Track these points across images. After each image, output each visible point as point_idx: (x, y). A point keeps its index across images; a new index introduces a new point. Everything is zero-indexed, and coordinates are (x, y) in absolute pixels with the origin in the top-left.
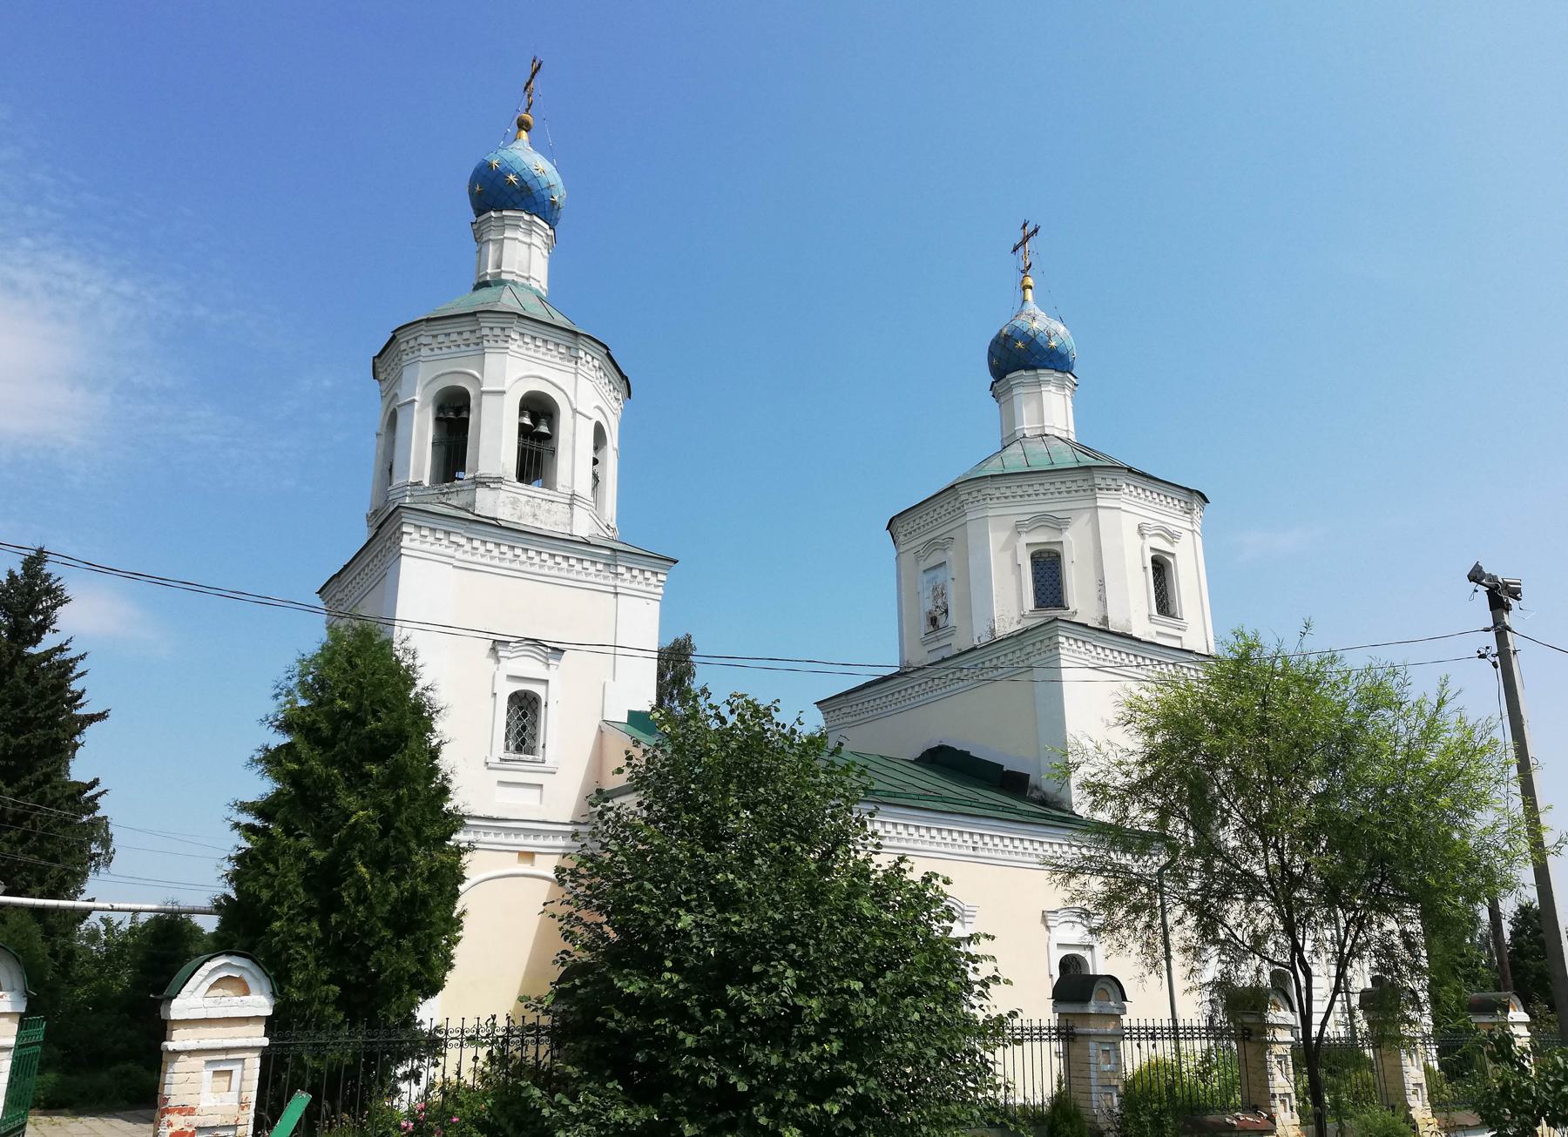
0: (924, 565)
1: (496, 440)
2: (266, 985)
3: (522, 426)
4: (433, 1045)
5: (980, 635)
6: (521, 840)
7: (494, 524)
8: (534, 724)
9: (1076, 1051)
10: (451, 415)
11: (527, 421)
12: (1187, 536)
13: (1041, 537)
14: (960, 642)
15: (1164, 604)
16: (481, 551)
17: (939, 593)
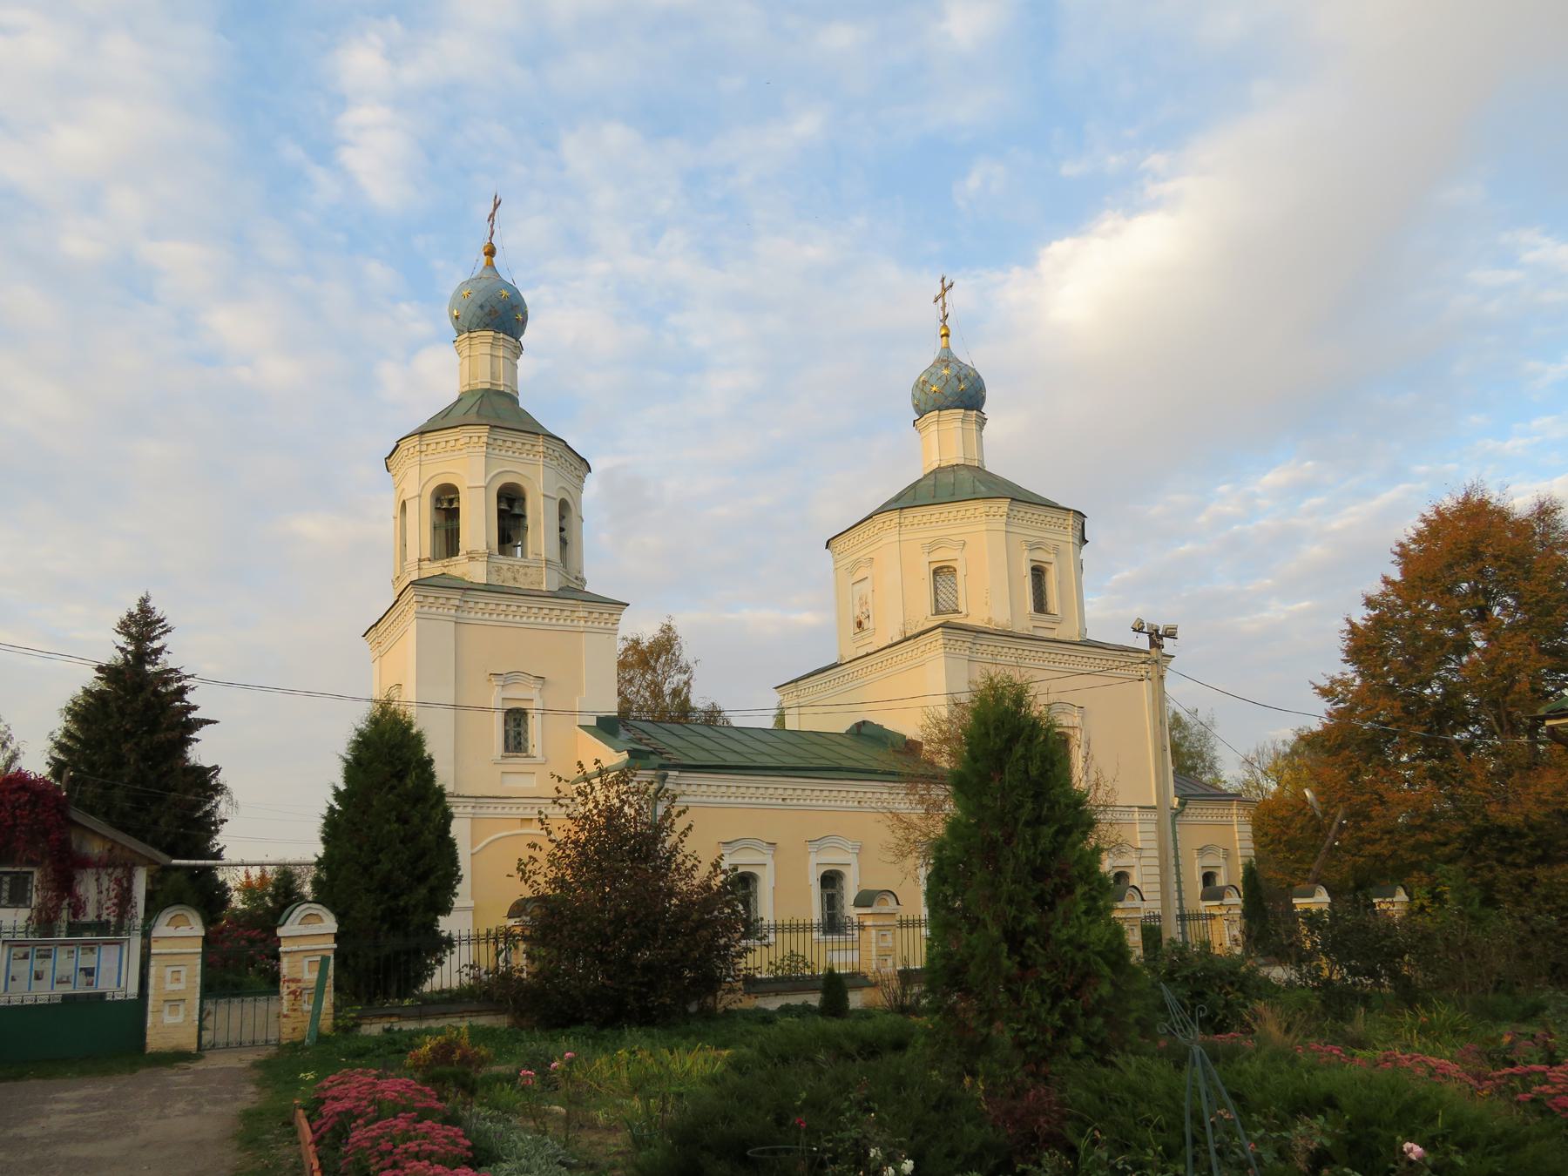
1: (477, 524)
2: (196, 914)
4: (449, 943)
11: (504, 506)
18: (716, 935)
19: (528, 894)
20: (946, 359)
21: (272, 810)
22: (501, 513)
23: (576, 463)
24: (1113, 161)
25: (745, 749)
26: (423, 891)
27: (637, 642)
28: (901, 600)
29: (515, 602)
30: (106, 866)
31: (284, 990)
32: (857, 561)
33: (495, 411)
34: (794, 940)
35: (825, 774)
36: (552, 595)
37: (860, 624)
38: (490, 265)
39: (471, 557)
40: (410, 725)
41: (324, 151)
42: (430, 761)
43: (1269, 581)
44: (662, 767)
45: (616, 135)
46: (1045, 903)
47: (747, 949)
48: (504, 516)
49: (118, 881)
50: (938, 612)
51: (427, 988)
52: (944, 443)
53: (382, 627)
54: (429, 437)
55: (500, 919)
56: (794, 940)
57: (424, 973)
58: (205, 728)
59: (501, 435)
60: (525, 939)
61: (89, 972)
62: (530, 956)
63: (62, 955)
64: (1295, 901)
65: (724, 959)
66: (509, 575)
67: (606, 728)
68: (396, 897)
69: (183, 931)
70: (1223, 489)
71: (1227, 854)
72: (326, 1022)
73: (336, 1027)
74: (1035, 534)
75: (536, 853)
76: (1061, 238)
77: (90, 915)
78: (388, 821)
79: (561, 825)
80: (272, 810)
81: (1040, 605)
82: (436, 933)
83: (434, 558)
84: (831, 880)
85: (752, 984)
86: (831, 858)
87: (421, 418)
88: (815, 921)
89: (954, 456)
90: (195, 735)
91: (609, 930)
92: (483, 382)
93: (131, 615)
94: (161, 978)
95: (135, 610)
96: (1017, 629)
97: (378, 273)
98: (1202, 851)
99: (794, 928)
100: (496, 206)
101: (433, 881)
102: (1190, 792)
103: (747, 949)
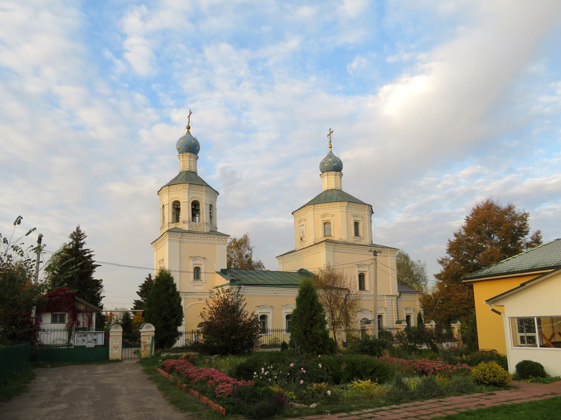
1: (185, 212)
4: (181, 334)
11: (193, 207)
18: (252, 332)
19: (203, 321)
20: (331, 155)
21: (119, 294)
22: (193, 209)
23: (214, 193)
24: (406, 57)
25: (265, 278)
26: (174, 320)
27: (235, 239)
28: (314, 233)
29: (197, 236)
30: (85, 312)
31: (142, 345)
32: (301, 220)
33: (190, 178)
36: (208, 233)
37: (301, 239)
38: (189, 132)
39: (184, 222)
40: (170, 275)
41: (119, 54)
42: (175, 285)
43: (463, 209)
44: (240, 285)
45: (225, 48)
46: (311, 325)
47: (261, 336)
48: (193, 204)
49: (88, 316)
50: (325, 236)
51: (175, 346)
52: (329, 182)
53: (157, 242)
54: (171, 187)
55: (195, 328)
57: (174, 342)
58: (97, 267)
59: (192, 186)
60: (202, 333)
61: (95, 340)
62: (204, 337)
63: (89, 335)
64: (459, 323)
65: (255, 338)
66: (195, 227)
67: (223, 272)
68: (167, 321)
69: (118, 330)
70: (447, 175)
71: (414, 310)
72: (153, 353)
73: (155, 354)
74: (355, 212)
75: (205, 310)
76: (387, 84)
77: (81, 325)
78: (165, 301)
79: (212, 304)
80: (119, 294)
81: (357, 233)
82: (177, 332)
83: (173, 223)
85: (264, 346)
87: (168, 181)
89: (332, 186)
90: (95, 270)
91: (224, 331)
92: (187, 169)
93: (74, 233)
94: (112, 341)
95: (75, 231)
96: (349, 241)
97: (140, 98)
98: (406, 309)
99: (278, 331)
100: (190, 114)
101: (177, 317)
102: (403, 291)
103: (261, 336)
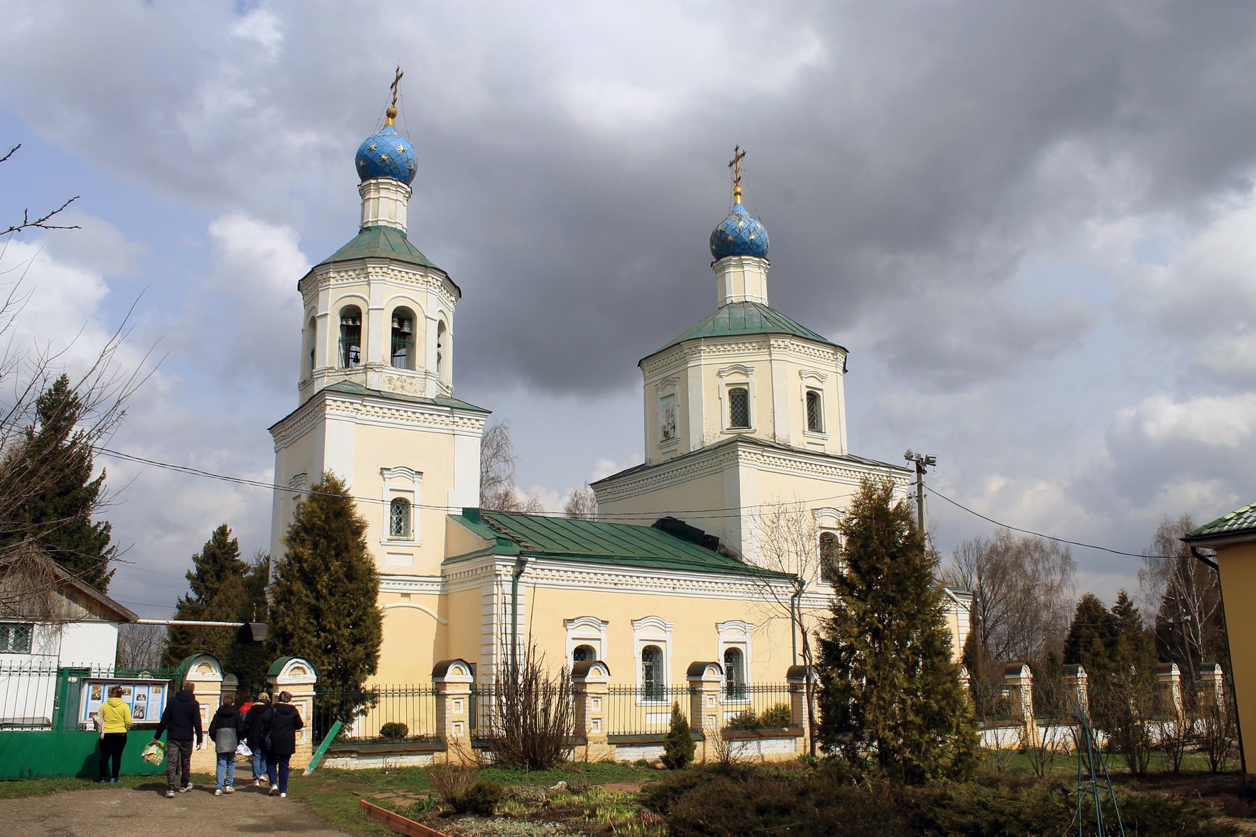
0: (661, 394)
3: (393, 329)
5: (694, 445)
6: (401, 586)
7: (379, 395)
8: (408, 520)
9: (695, 698)
10: (350, 323)
11: (396, 326)
12: (832, 377)
13: (738, 378)
14: (682, 450)
15: (814, 422)
16: (372, 410)
17: (670, 414)
34: (390, 705)
35: (648, 563)
37: (666, 433)
56: (390, 705)
69: (301, 678)
84: (651, 654)
86: (648, 634)
88: (639, 686)
100: (398, 78)
